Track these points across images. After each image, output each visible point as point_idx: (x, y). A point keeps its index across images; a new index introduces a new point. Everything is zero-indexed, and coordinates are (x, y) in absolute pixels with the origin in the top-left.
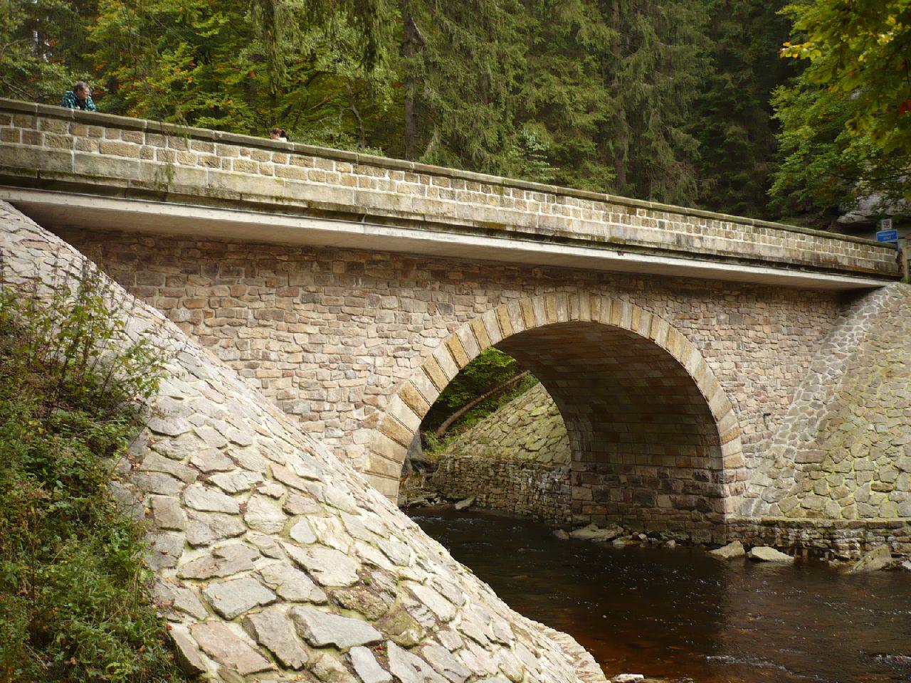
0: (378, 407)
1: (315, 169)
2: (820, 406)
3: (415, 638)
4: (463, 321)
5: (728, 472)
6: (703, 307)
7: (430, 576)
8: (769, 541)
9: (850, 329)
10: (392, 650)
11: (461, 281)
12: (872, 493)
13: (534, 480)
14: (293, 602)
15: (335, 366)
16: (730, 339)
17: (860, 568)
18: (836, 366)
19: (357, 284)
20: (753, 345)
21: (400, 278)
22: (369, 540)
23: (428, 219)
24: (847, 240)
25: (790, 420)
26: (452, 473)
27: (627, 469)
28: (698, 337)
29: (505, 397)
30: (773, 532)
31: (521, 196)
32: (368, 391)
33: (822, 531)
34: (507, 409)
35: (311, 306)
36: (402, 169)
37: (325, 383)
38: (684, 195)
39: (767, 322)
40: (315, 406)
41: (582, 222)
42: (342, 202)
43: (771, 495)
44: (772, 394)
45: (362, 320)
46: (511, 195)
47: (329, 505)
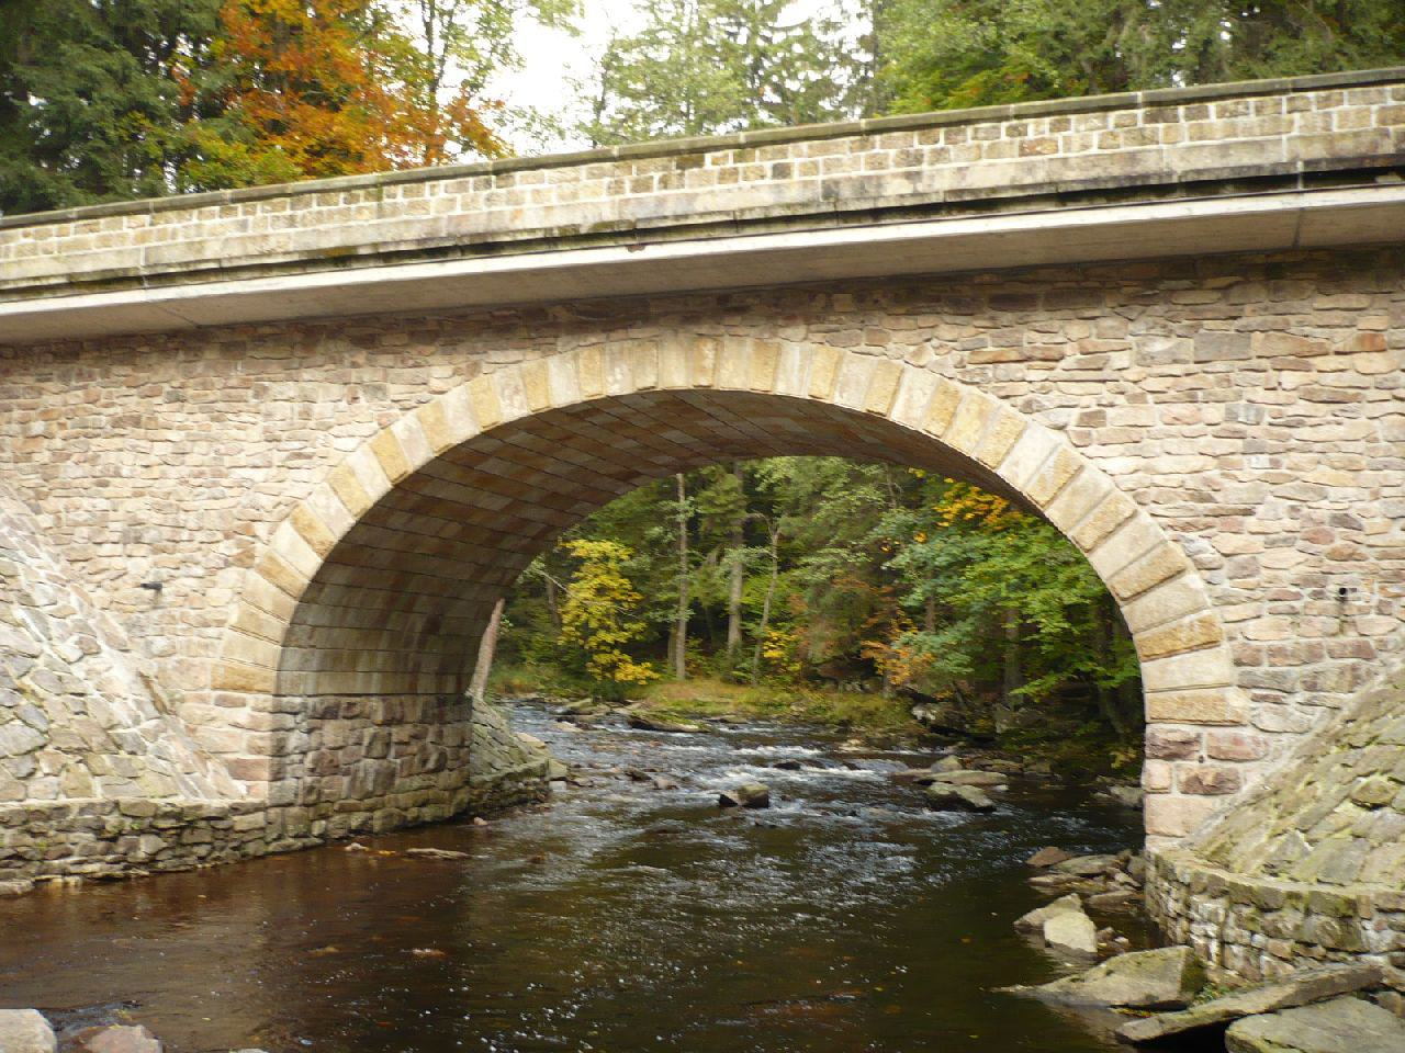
23: (226, 264)
31: (419, 194)
36: (214, 203)
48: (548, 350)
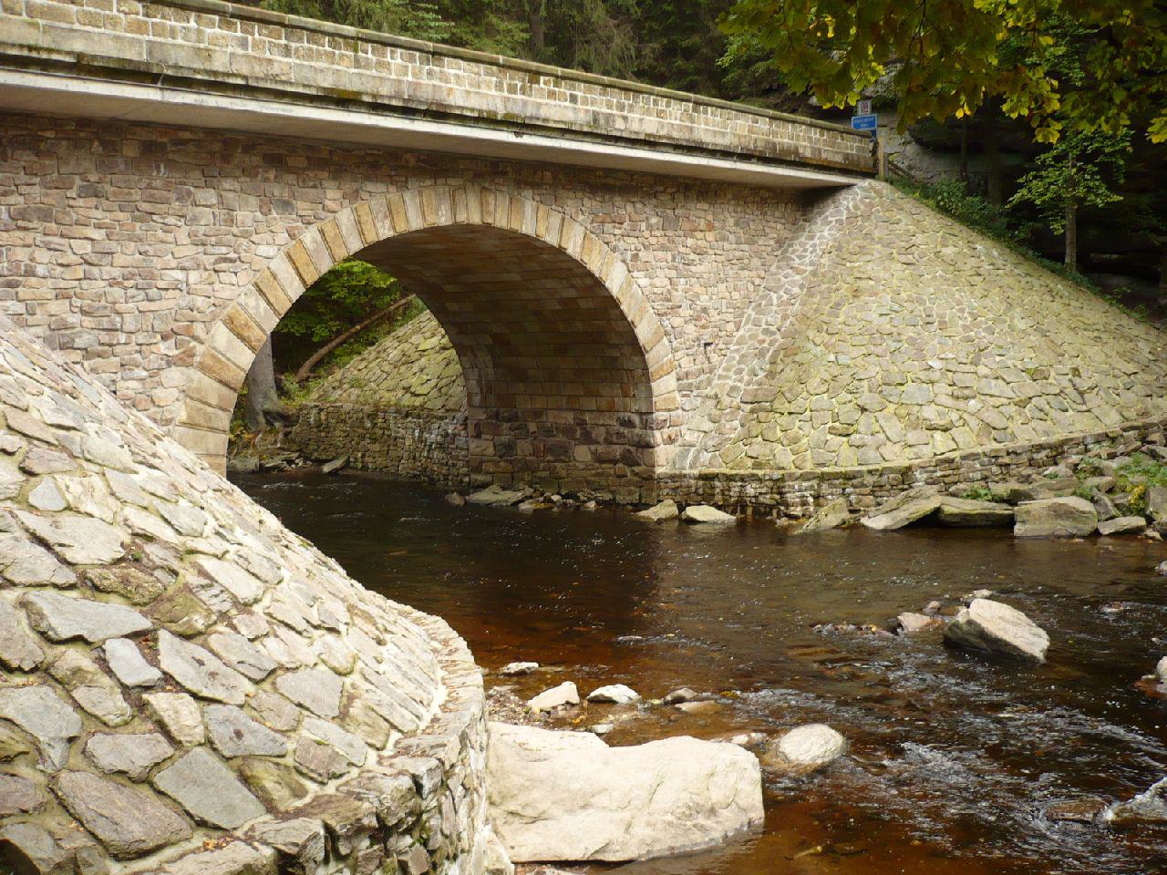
0: (195, 338)
1: (85, 8)
2: (773, 333)
3: (199, 623)
4: (309, 223)
5: (659, 415)
6: (629, 208)
7: (232, 549)
8: (706, 499)
9: (812, 238)
10: (165, 640)
11: (304, 169)
12: (829, 437)
13: (421, 432)
14: (26, 586)
15: (131, 283)
16: (663, 248)
17: (811, 527)
18: (793, 282)
19: (159, 171)
20: (692, 256)
21: (218, 163)
22: (145, 504)
23: (252, 83)
24: (811, 125)
25: (737, 351)
26: (318, 427)
27: (537, 414)
28: (621, 245)
29: (386, 327)
30: (713, 488)
31: (384, 55)
32: (178, 317)
33: (770, 484)
34: (388, 342)
35: (93, 201)
37: (1000, 460)
38: (617, 63)
39: (711, 227)
40: (105, 337)
41: (468, 92)
42: (128, 56)
43: (710, 443)
44: (715, 317)
45: (166, 221)
46: (368, 53)
47: (89, 461)
48: (403, 186)
